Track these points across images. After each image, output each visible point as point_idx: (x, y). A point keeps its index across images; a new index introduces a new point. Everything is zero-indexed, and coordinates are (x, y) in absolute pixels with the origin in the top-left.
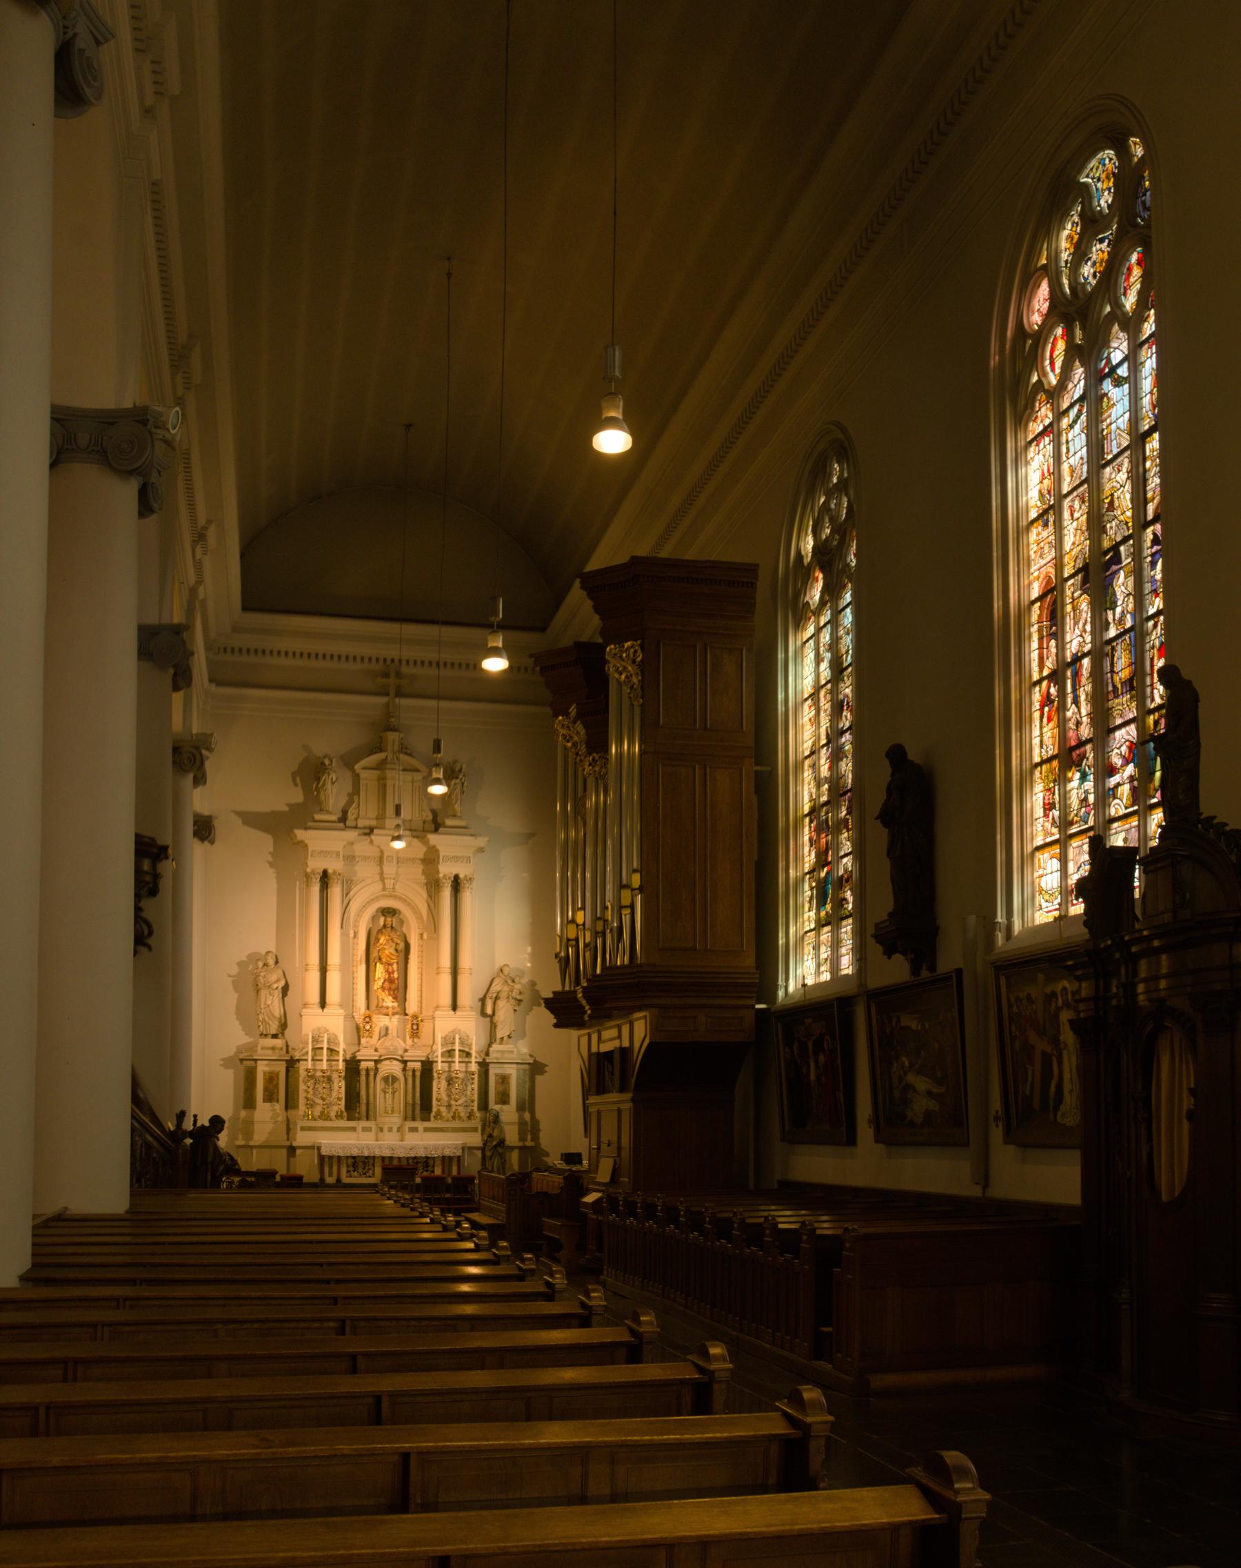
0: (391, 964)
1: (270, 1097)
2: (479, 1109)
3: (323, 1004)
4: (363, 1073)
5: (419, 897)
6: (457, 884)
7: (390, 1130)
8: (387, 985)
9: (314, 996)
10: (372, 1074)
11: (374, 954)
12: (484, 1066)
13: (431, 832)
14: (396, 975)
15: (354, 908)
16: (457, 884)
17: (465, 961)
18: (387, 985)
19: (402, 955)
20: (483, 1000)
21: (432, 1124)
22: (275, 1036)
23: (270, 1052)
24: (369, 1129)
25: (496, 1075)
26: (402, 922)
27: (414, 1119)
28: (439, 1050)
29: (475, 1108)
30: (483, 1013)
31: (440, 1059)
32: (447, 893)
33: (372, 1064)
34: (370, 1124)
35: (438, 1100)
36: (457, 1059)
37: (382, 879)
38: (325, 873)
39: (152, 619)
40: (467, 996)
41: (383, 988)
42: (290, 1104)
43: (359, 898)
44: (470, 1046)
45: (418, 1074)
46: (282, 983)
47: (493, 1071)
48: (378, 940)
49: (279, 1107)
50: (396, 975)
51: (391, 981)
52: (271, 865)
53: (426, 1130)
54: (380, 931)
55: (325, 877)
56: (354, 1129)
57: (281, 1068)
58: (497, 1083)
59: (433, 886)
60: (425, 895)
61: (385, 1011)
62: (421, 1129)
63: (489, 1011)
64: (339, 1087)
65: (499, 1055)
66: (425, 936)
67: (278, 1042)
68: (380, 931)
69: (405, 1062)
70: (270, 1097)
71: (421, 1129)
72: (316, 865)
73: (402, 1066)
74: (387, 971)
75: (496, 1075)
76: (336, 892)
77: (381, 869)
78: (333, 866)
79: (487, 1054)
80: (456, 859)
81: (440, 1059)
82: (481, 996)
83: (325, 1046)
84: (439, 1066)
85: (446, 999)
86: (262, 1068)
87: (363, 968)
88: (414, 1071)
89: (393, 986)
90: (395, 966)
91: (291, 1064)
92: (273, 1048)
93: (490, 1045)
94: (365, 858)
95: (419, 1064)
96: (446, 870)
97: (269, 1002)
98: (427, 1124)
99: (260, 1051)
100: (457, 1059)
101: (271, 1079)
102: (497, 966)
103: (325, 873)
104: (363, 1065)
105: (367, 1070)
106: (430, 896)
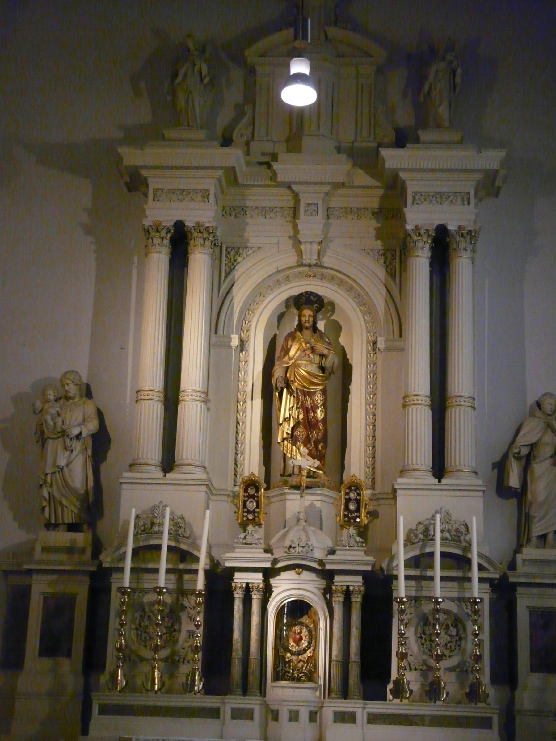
0: (311, 394)
1: (53, 646)
2: (494, 680)
3: (169, 463)
4: (238, 596)
5: (370, 275)
6: (442, 245)
7: (294, 716)
8: (301, 432)
9: (151, 447)
10: (256, 598)
11: (278, 373)
12: (504, 591)
13: (390, 146)
14: (320, 414)
15: (239, 297)
16: (442, 245)
17: (461, 382)
18: (301, 432)
19: (335, 382)
20: (501, 467)
21: (391, 706)
22: (73, 528)
23: (64, 557)
24: (247, 714)
25: (533, 611)
26: (337, 328)
27: (345, 694)
28: (402, 554)
29: (486, 678)
30: (502, 489)
31: (402, 572)
32: (420, 264)
33: (257, 579)
34: (252, 702)
35: (402, 657)
36: (438, 572)
37: (297, 242)
38: (179, 226)
39: (470, 583)
40: (464, 447)
41: (293, 438)
42: (93, 662)
43: (248, 276)
44: (468, 548)
45: (357, 599)
46: (93, 426)
47: (524, 602)
48: (287, 351)
49: (69, 669)
50: (320, 414)
51: (309, 424)
52: (88, 230)
53: (373, 719)
54: (291, 336)
55: (180, 242)
56: (214, 713)
57: (81, 590)
58: (533, 625)
59: (395, 257)
60: (381, 273)
61: (294, 480)
62: (361, 716)
63: (514, 481)
64: (193, 627)
65: (534, 570)
66: (381, 345)
67: (81, 538)
68: (291, 336)
69: (328, 576)
70: (53, 646)
71: (361, 716)
72: (163, 213)
73: (322, 583)
74: (301, 406)
75: (533, 611)
76: (199, 265)
77: (295, 226)
78: (198, 214)
79: (512, 566)
80: (440, 197)
81: (402, 572)
82: (498, 458)
83: (165, 543)
84: (402, 589)
85: (421, 451)
86: (40, 588)
87: (258, 403)
88: (348, 593)
89: (314, 435)
90: (319, 398)
91: (100, 582)
92: (70, 550)
93: (518, 550)
94: (265, 211)
95: (360, 579)
96: (420, 217)
97: (62, 462)
98: (376, 707)
99: (38, 554)
100: (438, 572)
101: (58, 608)
102: (531, 399)
103: (179, 226)
104: (240, 579)
105: (248, 590)
106: (391, 274)
